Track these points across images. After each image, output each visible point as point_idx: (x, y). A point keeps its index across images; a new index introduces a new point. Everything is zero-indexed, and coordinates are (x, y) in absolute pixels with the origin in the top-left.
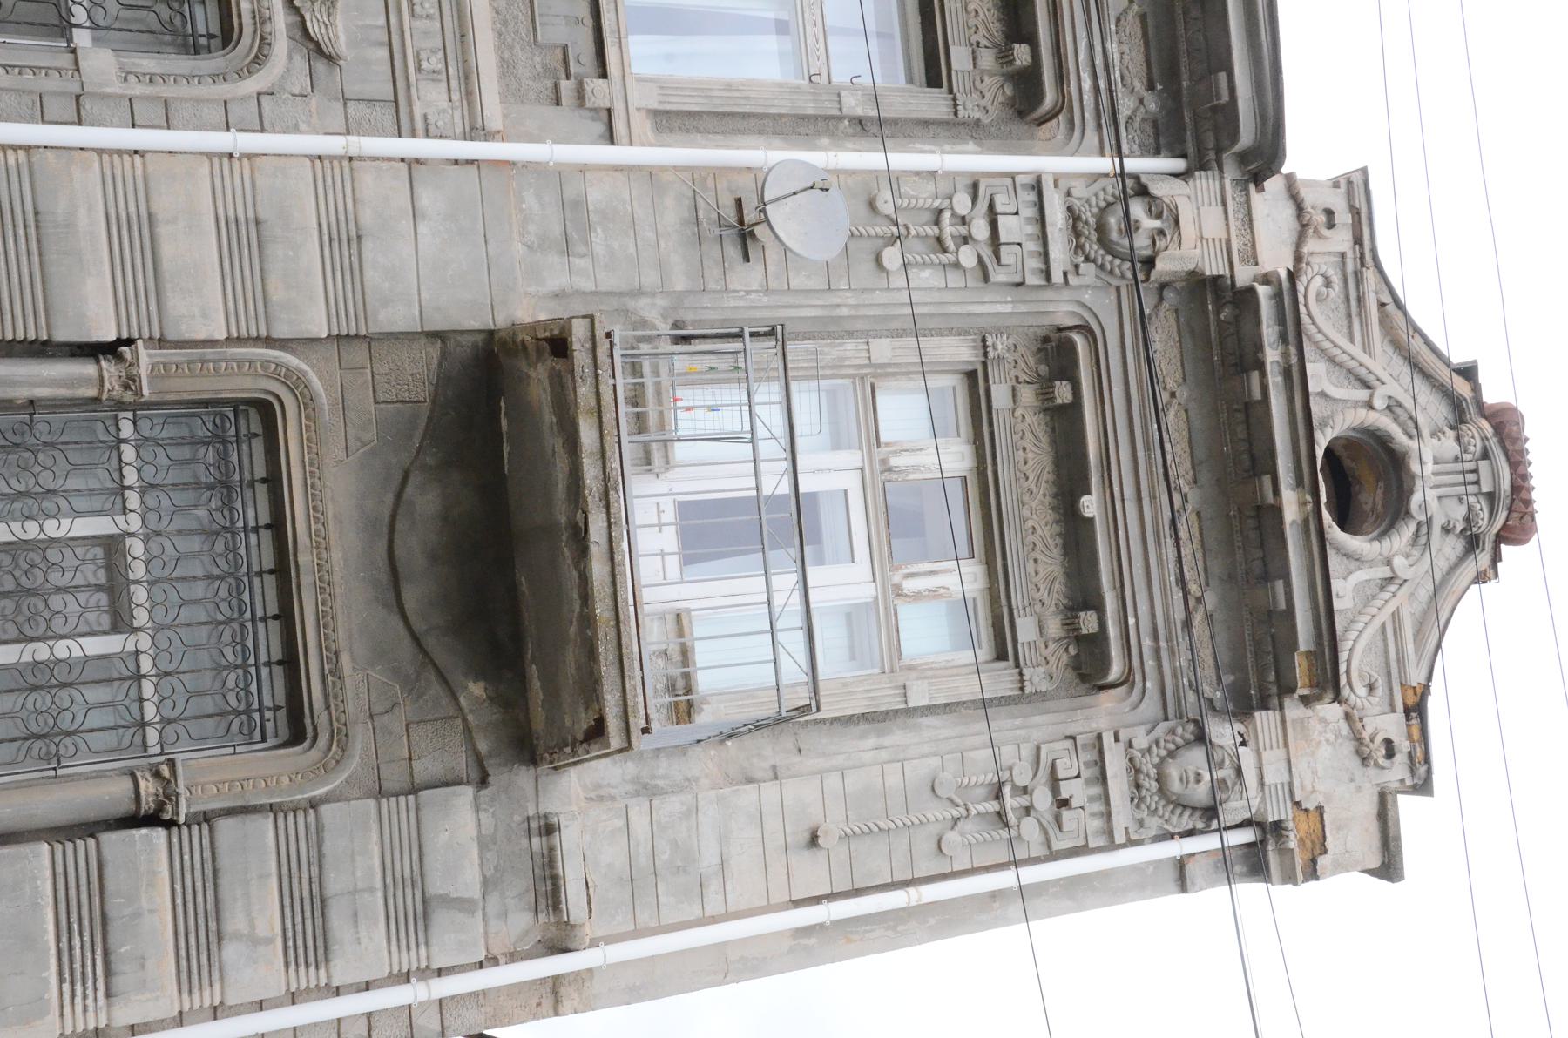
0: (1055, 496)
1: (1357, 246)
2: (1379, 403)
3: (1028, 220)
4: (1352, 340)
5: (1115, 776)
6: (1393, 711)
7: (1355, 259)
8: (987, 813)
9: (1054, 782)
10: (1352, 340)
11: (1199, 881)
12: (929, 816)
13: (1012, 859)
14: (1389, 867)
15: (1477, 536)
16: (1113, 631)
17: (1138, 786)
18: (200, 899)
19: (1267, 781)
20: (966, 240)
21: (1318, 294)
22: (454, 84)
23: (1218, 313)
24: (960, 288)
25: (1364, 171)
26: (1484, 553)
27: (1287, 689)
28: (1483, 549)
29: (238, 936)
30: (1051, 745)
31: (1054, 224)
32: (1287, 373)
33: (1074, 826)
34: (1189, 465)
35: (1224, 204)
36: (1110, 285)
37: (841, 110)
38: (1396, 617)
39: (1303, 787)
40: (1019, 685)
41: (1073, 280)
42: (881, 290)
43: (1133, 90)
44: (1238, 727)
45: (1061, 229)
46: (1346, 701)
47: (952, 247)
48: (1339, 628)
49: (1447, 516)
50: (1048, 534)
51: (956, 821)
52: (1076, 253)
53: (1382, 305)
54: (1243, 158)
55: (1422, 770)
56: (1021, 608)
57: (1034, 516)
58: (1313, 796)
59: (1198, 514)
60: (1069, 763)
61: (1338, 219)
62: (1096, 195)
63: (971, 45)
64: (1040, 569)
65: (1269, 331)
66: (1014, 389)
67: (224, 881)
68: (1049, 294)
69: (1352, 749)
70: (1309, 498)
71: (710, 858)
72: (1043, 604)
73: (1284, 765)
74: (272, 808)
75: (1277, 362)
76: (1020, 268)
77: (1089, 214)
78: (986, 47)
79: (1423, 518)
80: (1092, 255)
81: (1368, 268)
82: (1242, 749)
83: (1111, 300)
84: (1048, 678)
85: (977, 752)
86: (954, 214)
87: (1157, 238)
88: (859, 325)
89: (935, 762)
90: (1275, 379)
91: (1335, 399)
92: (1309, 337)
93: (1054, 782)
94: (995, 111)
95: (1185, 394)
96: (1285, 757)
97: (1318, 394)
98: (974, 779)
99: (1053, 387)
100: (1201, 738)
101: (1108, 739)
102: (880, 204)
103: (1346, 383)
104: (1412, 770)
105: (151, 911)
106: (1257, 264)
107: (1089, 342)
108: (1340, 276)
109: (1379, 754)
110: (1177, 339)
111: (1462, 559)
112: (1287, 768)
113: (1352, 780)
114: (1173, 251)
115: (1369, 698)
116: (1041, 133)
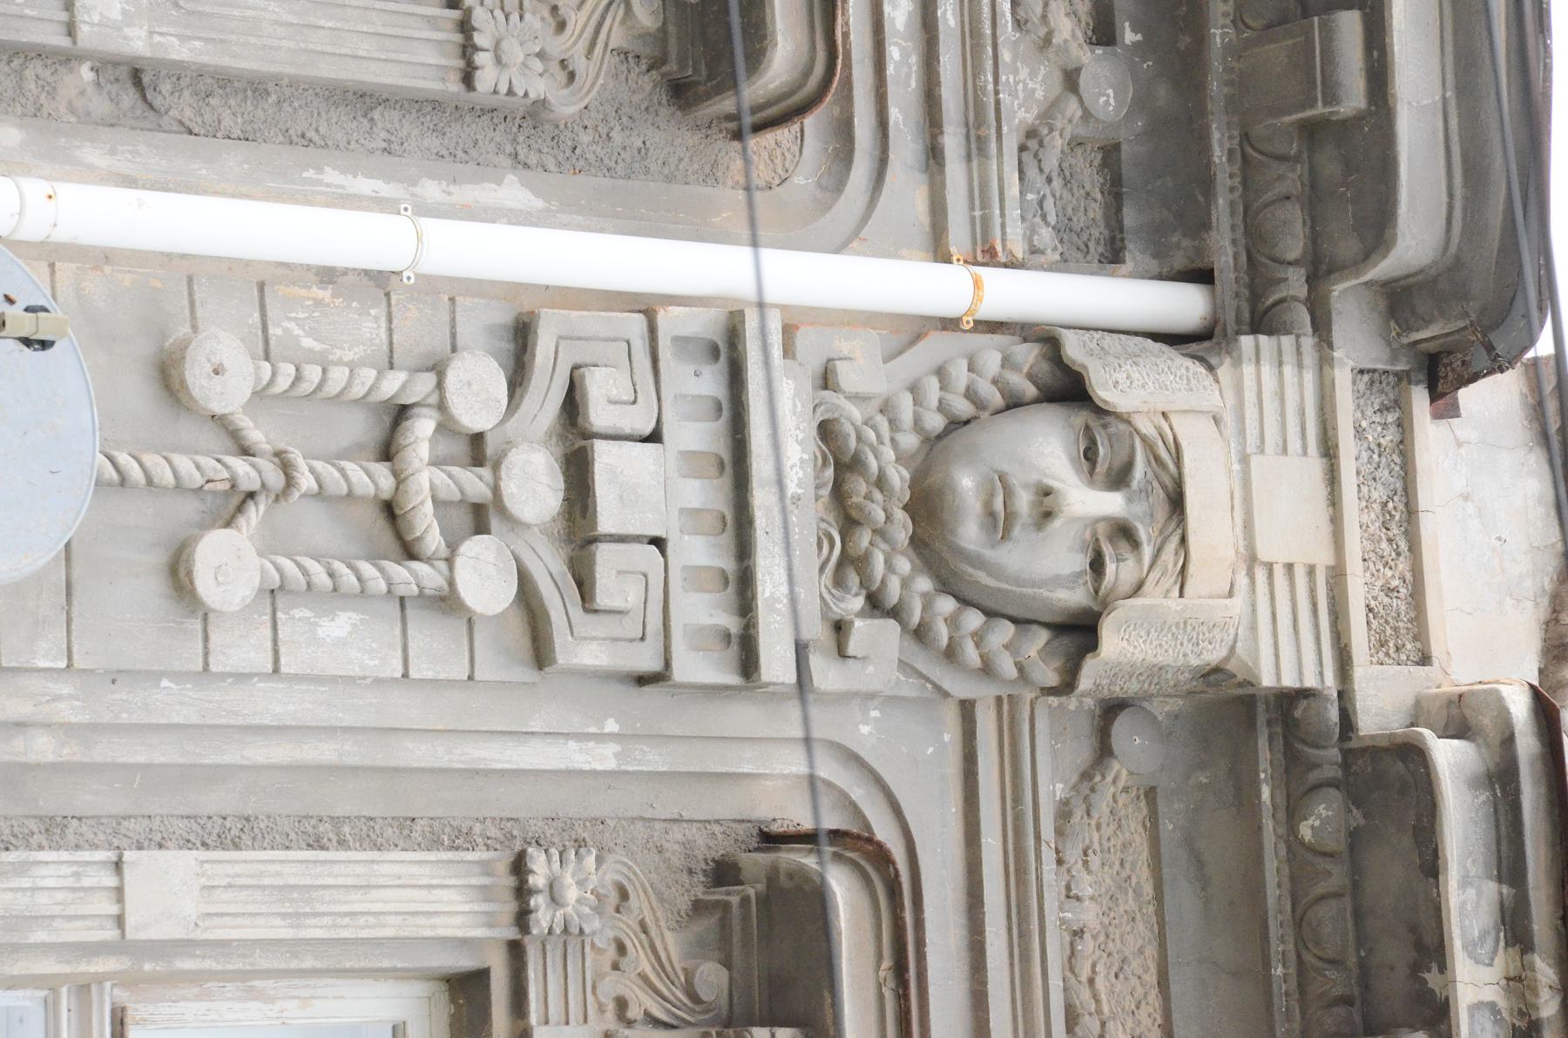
23: (1292, 813)
24: (451, 683)
35: (1329, 451)
42: (176, 676)
43: (1047, 41)
52: (839, 581)
77: (889, 454)
80: (893, 593)
86: (447, 426)
87: (1107, 550)
102: (197, 377)
106: (1425, 660)
110: (1148, 889)
114: (1159, 598)
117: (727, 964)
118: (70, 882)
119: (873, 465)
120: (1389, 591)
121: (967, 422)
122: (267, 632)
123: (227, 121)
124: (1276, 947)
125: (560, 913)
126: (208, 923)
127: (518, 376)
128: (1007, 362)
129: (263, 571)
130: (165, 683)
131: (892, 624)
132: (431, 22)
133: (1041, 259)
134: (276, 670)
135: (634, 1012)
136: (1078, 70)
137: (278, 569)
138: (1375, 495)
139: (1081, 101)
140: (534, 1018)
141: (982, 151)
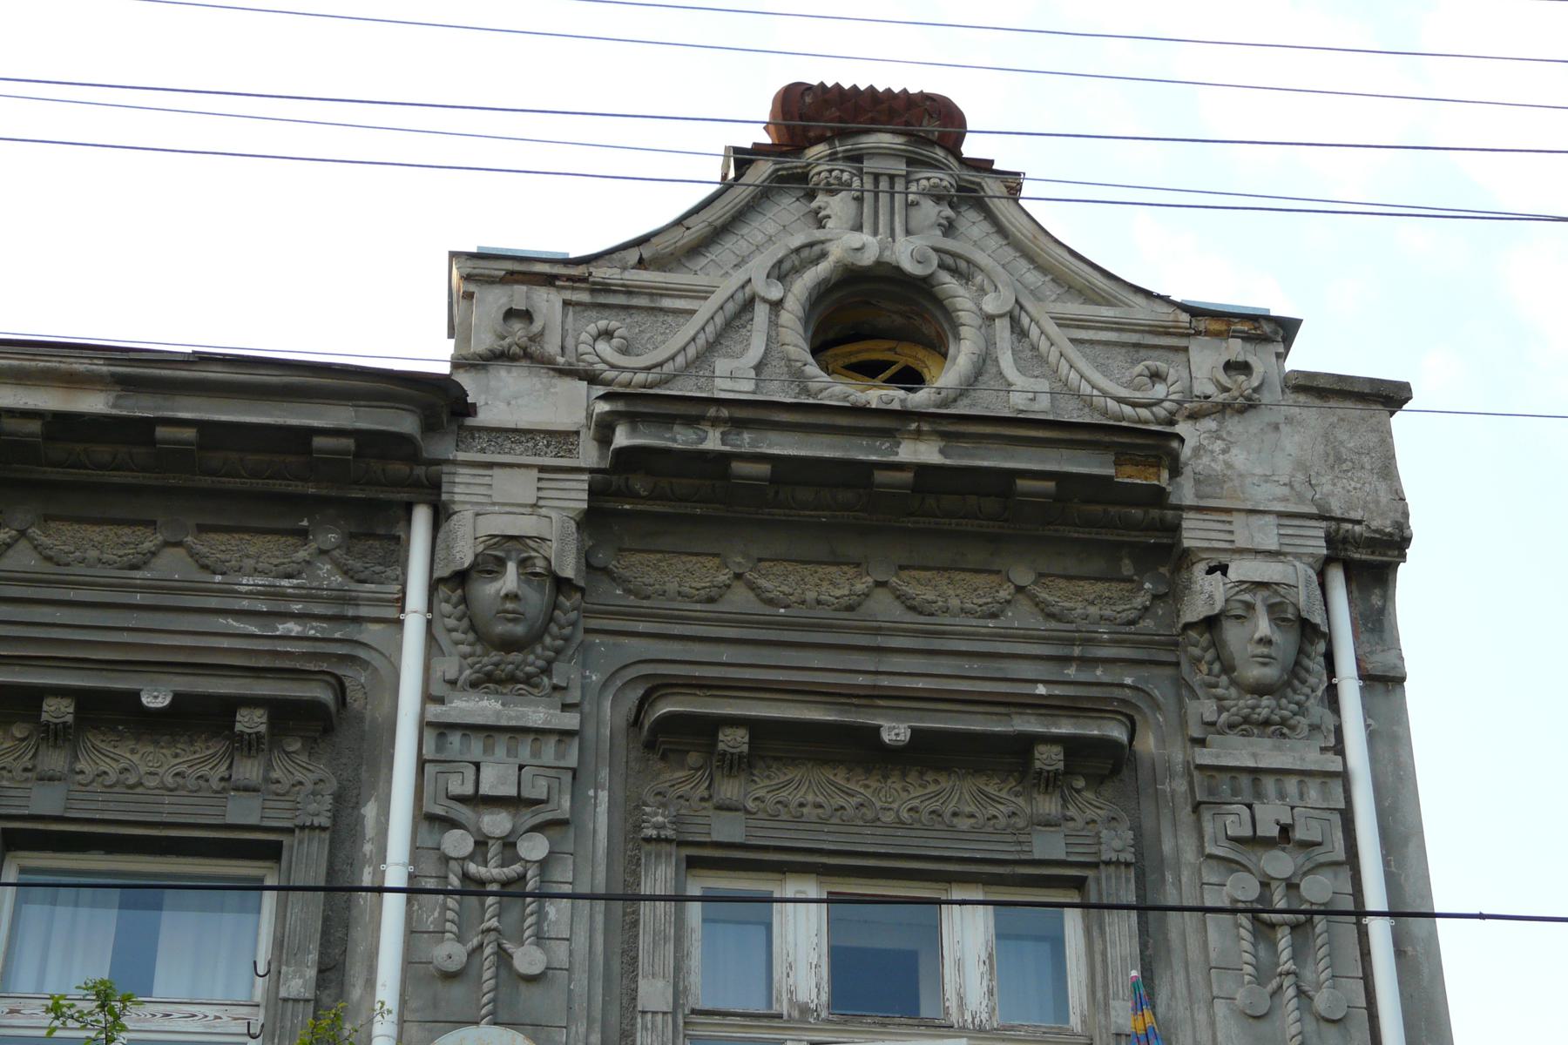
0: (868, 771)
1: (558, 283)
2: (775, 293)
3: (488, 750)
5: (1255, 755)
6: (1186, 349)
7: (573, 289)
8: (1292, 945)
9: (1255, 842)
10: (692, 312)
11: (1390, 658)
12: (1294, 1029)
13: (1353, 919)
14: (1392, 396)
15: (960, 189)
16: (1065, 728)
17: (1266, 723)
19: (1274, 547)
20: (509, 844)
21: (624, 351)
23: (634, 496)
24: (574, 863)
25: (454, 255)
26: (983, 184)
27: (1158, 496)
28: (979, 184)
30: (1206, 839)
31: (498, 714)
32: (739, 424)
33: (1314, 823)
34: (833, 569)
35: (490, 465)
36: (582, 642)
37: (307, 1001)
38: (1063, 322)
39: (1285, 499)
40: (1123, 867)
41: (574, 696)
42: (570, 980)
43: (308, 562)
44: (1199, 570)
45: (503, 705)
46: (1172, 414)
47: (517, 868)
48: (1097, 419)
49: (931, 226)
50: (920, 792)
51: (1301, 993)
52: (536, 686)
53: (641, 264)
54: (431, 426)
55: (1267, 328)
56: (1019, 848)
57: (895, 806)
58: (1297, 485)
59: (902, 568)
60: (1232, 818)
61: (520, 305)
62: (457, 643)
63: (224, 790)
64: (967, 809)
65: (682, 439)
66: (720, 808)
68: (590, 732)
69: (1236, 419)
70: (914, 426)
72: (1014, 814)
73: (1254, 519)
75: (723, 434)
76: (552, 773)
77: (485, 660)
78: (230, 767)
79: (935, 260)
80: (541, 663)
81: (590, 274)
82: (1233, 574)
83: (602, 644)
84: (1114, 824)
85: (1211, 945)
86: (471, 857)
87: (529, 570)
88: (614, 1018)
89: (1220, 1008)
90: (746, 442)
91: (766, 349)
93: (1255, 842)
94: (321, 769)
95: (739, 559)
96: (1242, 516)
97: (759, 379)
98: (1247, 957)
99: (724, 753)
100: (1211, 623)
101: (1205, 757)
102: (453, 967)
103: (743, 331)
104: (1265, 339)
106: (577, 433)
107: (667, 694)
108: (594, 314)
109: (1245, 386)
110: (659, 556)
111: (990, 216)
112: (1259, 516)
113: (1276, 427)
114: (552, 550)
115: (1170, 380)
116: (356, 705)
117: (688, 752)
118: (649, 1033)
119: (490, 667)
120: (548, 446)
121: (471, 621)
122: (553, 942)
123: (339, 935)
124: (689, 511)
125: (668, 825)
126: (667, 975)
127: (452, 824)
128: (447, 601)
129: (531, 944)
130: (572, 987)
131: (555, 666)
132: (301, 842)
133: (401, 577)
134: (568, 940)
135: (706, 794)
136: (319, 549)
137: (529, 937)
138: (508, 446)
139: (334, 549)
140: (708, 840)
141: (356, 599)
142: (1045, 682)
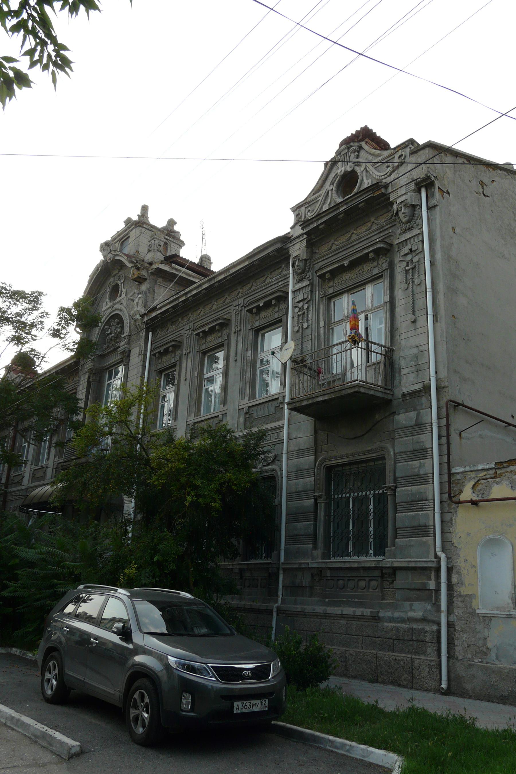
4: (319, 201)
16: (371, 249)
17: (409, 229)
18: (410, 480)
22: (279, 431)
25: (290, 209)
29: (419, 471)
67: (408, 475)
71: (415, 351)
74: (395, 463)
92: (319, 212)
93: (406, 255)
105: (411, 491)
114: (409, 201)
142: (378, 238)
